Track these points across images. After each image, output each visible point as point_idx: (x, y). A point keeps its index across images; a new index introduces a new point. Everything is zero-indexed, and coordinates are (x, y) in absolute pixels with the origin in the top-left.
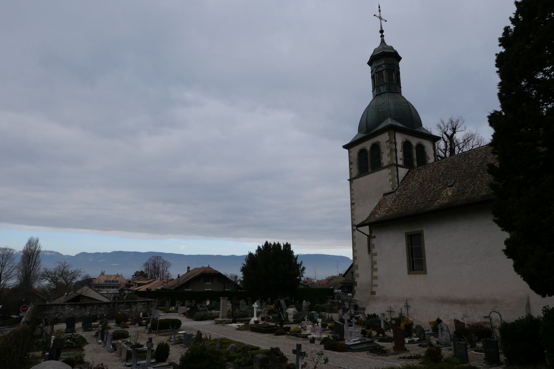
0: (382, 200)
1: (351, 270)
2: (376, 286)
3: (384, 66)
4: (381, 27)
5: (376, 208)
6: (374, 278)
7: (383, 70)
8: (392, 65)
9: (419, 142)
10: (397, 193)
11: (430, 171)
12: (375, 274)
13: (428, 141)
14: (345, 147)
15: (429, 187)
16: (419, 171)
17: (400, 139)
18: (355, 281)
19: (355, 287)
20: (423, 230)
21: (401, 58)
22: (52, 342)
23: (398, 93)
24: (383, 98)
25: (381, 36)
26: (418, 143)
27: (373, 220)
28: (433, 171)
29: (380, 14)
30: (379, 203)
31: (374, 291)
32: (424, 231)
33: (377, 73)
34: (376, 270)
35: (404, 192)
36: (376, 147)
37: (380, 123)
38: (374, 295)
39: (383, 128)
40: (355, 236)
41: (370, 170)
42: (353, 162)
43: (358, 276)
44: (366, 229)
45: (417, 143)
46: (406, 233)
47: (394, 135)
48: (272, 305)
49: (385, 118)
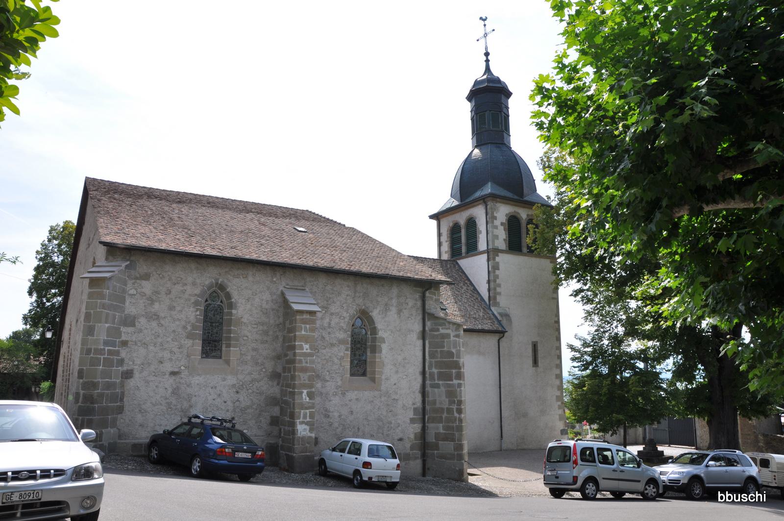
4: (486, 48)
14: (432, 217)
17: (503, 212)
21: (512, 94)
22: (779, 435)
23: (502, 144)
25: (485, 61)
36: (471, 223)
41: (464, 255)
48: (606, 225)
49: (480, 185)
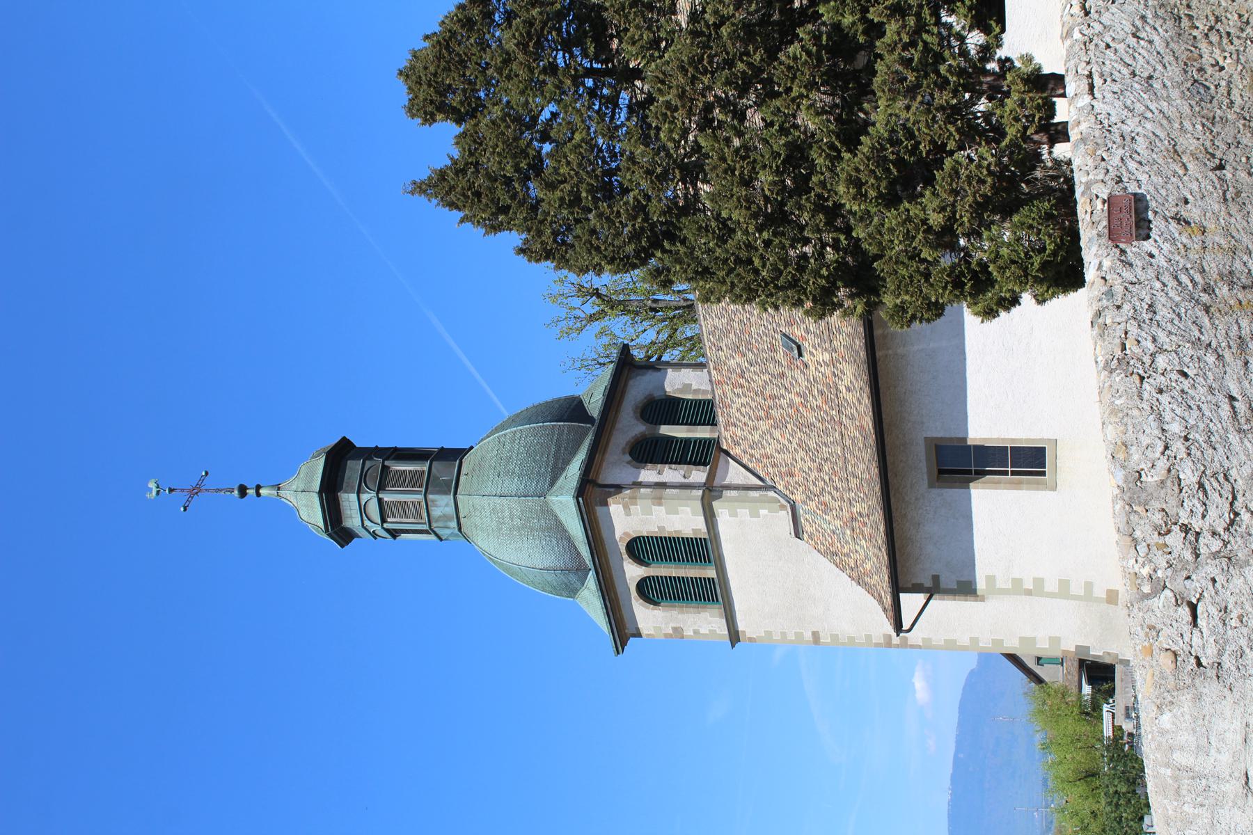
0: (816, 543)
1: (1031, 664)
2: (1089, 586)
3: (365, 497)
5: (841, 566)
6: (1064, 590)
7: (380, 500)
8: (366, 469)
9: (635, 412)
10: (798, 497)
11: (739, 396)
12: (1051, 586)
13: (631, 382)
15: (791, 405)
16: (735, 425)
18: (1073, 649)
19: (1091, 653)
20: (925, 438)
24: (475, 509)
26: (639, 415)
27: (882, 580)
28: (742, 386)
29: (182, 490)
30: (825, 554)
31: (1107, 595)
32: (929, 434)
33: (383, 520)
34: (1039, 582)
35: (799, 478)
36: (639, 549)
37: (559, 529)
38: (1120, 595)
39: (595, 519)
40: (923, 639)
41: (711, 573)
42: (674, 626)
43: (1055, 640)
44: (911, 602)
45: (638, 420)
46: (931, 486)
47: (607, 490)
49: (548, 512)
